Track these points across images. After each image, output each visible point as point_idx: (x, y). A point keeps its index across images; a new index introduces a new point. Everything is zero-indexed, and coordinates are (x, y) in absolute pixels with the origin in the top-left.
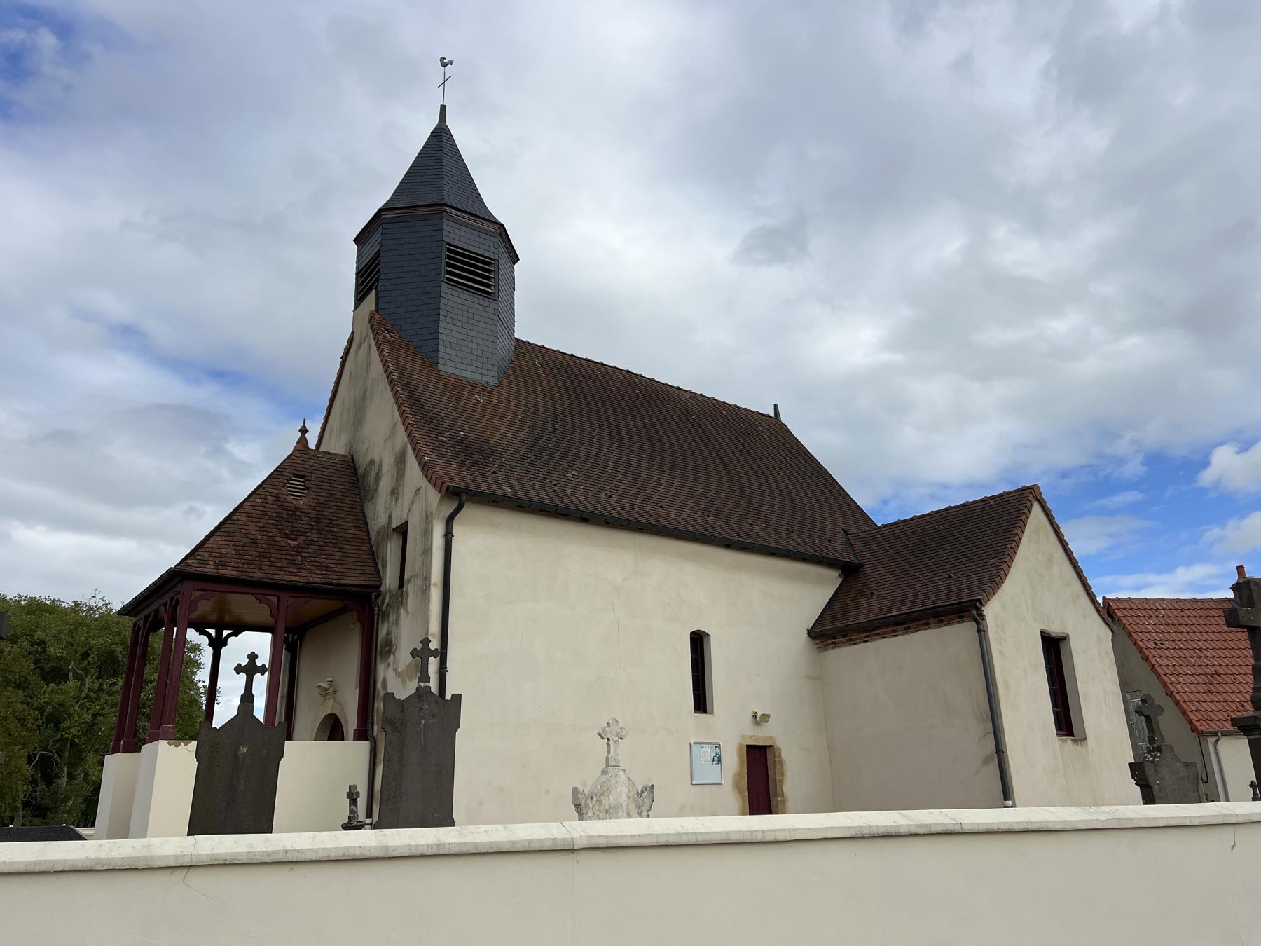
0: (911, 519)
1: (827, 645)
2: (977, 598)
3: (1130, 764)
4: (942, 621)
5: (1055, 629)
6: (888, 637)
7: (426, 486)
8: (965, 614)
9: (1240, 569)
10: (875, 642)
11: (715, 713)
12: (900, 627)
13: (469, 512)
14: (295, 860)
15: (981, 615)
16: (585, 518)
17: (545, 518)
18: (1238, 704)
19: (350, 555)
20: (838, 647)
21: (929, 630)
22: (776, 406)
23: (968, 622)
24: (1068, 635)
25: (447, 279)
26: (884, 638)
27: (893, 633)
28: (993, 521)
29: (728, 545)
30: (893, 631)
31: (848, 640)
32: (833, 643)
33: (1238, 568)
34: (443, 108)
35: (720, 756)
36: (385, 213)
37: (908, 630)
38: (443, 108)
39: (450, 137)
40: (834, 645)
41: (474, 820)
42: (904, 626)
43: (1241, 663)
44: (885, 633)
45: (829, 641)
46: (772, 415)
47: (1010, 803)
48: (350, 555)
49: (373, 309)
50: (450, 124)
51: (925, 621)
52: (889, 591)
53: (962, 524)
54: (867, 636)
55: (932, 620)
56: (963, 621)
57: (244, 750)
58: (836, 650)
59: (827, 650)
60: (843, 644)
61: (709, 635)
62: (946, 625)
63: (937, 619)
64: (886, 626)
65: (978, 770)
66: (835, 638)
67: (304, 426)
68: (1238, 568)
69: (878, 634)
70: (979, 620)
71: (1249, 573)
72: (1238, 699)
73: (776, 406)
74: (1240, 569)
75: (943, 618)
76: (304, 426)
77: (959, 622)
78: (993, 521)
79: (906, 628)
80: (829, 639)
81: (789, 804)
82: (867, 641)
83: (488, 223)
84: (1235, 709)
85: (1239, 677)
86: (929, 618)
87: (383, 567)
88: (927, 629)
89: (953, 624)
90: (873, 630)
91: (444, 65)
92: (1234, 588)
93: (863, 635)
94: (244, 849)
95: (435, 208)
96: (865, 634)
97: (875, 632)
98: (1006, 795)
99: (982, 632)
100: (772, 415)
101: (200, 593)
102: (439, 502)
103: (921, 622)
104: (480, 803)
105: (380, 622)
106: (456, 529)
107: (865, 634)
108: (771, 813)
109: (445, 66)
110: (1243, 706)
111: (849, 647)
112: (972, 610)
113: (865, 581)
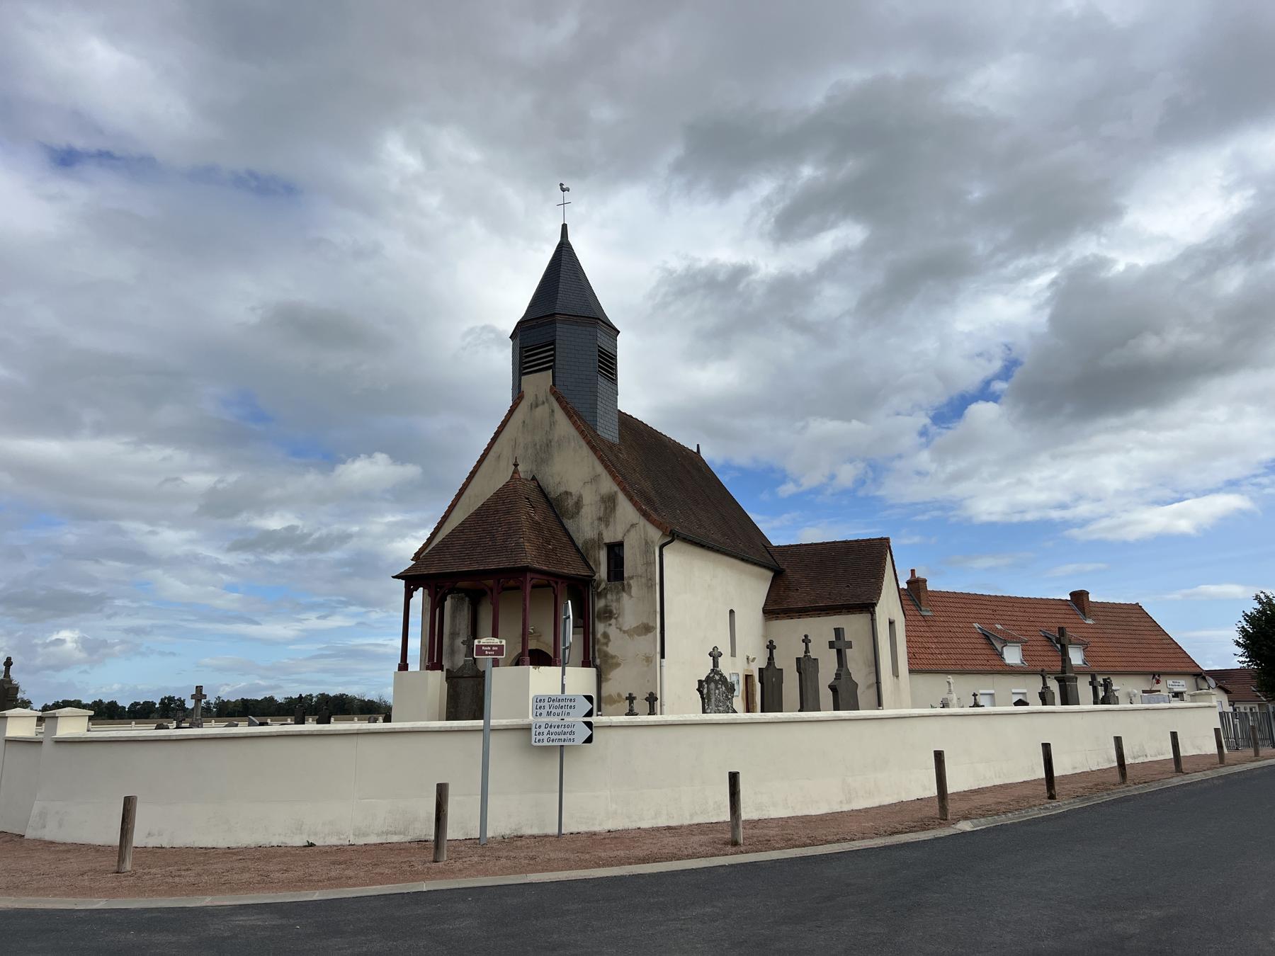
0: (811, 544)
3: (301, 695)
5: (892, 618)
7: (644, 526)
9: (913, 571)
11: (795, 660)
13: (676, 544)
15: (874, 611)
17: (689, 545)
19: (1039, 648)
24: (894, 621)
25: (599, 371)
29: (743, 560)
33: (912, 570)
34: (564, 227)
37: (828, 614)
38: (564, 227)
39: (1178, 650)
40: (777, 618)
41: (672, 713)
45: (774, 616)
46: (695, 450)
47: (881, 708)
48: (1039, 648)
49: (551, 384)
59: (772, 620)
60: (783, 618)
64: (815, 610)
67: (516, 461)
68: (912, 570)
70: (873, 614)
76: (516, 461)
90: (805, 612)
91: (563, 190)
92: (908, 583)
94: (470, 725)
99: (873, 620)
100: (695, 450)
105: (596, 599)
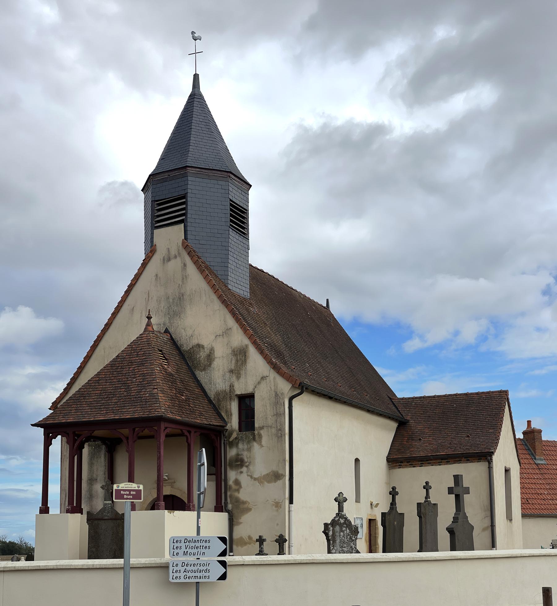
1: (396, 466)
2: (491, 451)
4: (469, 460)
5: (508, 466)
6: (435, 465)
7: (274, 378)
8: (482, 458)
9: (529, 422)
10: (427, 467)
11: (361, 502)
12: (444, 460)
13: (305, 396)
14: (396, 561)
15: (491, 459)
16: (330, 398)
18: (525, 499)
20: (403, 468)
21: (460, 464)
22: (327, 300)
23: (483, 462)
26: (433, 465)
27: (438, 463)
28: (487, 408)
29: (368, 411)
30: (439, 462)
31: (410, 465)
32: (399, 465)
34: (196, 77)
35: (362, 524)
36: (190, 169)
37: (448, 463)
38: (196, 77)
40: (400, 466)
42: (446, 460)
43: (526, 477)
44: (434, 463)
45: (398, 464)
46: (325, 305)
50: (204, 89)
51: (459, 459)
52: (430, 439)
53: (468, 405)
54: (423, 464)
55: (463, 459)
56: (480, 461)
57: (395, 523)
58: (401, 469)
60: (406, 466)
61: (360, 461)
62: (470, 462)
63: (466, 459)
64: (436, 459)
65: (479, 534)
66: (402, 462)
67: (149, 314)
69: (430, 463)
70: (490, 462)
71: (533, 426)
72: (526, 497)
73: (327, 300)
74: (529, 422)
75: (470, 459)
76: (149, 314)
77: (478, 462)
78: (487, 408)
79: (447, 462)
80: (398, 463)
81: (293, 553)
82: (422, 466)
83: (245, 184)
84: (524, 502)
85: (525, 485)
86: (462, 458)
87: (227, 416)
88: (460, 463)
89: (474, 462)
90: (428, 461)
93: (420, 463)
95: (223, 173)
96: (421, 462)
97: (428, 462)
98: (493, 545)
99: (490, 468)
101: (138, 428)
102: (291, 388)
103: (456, 459)
104: (301, 545)
106: (294, 402)
107: (421, 462)
108: (456, 551)
109: (195, 40)
110: (527, 501)
111: (410, 468)
112: (488, 457)
113: (412, 431)
